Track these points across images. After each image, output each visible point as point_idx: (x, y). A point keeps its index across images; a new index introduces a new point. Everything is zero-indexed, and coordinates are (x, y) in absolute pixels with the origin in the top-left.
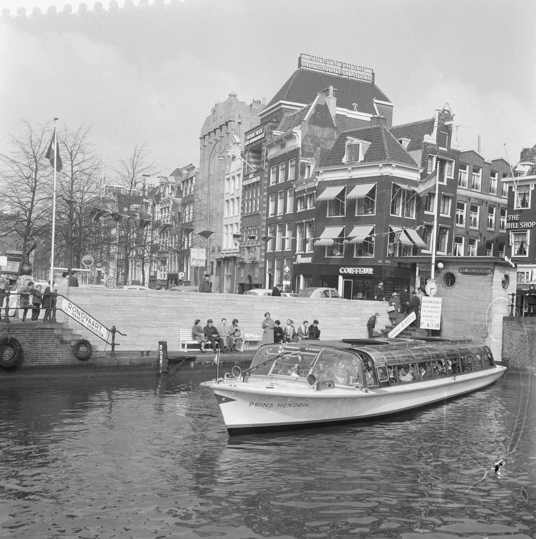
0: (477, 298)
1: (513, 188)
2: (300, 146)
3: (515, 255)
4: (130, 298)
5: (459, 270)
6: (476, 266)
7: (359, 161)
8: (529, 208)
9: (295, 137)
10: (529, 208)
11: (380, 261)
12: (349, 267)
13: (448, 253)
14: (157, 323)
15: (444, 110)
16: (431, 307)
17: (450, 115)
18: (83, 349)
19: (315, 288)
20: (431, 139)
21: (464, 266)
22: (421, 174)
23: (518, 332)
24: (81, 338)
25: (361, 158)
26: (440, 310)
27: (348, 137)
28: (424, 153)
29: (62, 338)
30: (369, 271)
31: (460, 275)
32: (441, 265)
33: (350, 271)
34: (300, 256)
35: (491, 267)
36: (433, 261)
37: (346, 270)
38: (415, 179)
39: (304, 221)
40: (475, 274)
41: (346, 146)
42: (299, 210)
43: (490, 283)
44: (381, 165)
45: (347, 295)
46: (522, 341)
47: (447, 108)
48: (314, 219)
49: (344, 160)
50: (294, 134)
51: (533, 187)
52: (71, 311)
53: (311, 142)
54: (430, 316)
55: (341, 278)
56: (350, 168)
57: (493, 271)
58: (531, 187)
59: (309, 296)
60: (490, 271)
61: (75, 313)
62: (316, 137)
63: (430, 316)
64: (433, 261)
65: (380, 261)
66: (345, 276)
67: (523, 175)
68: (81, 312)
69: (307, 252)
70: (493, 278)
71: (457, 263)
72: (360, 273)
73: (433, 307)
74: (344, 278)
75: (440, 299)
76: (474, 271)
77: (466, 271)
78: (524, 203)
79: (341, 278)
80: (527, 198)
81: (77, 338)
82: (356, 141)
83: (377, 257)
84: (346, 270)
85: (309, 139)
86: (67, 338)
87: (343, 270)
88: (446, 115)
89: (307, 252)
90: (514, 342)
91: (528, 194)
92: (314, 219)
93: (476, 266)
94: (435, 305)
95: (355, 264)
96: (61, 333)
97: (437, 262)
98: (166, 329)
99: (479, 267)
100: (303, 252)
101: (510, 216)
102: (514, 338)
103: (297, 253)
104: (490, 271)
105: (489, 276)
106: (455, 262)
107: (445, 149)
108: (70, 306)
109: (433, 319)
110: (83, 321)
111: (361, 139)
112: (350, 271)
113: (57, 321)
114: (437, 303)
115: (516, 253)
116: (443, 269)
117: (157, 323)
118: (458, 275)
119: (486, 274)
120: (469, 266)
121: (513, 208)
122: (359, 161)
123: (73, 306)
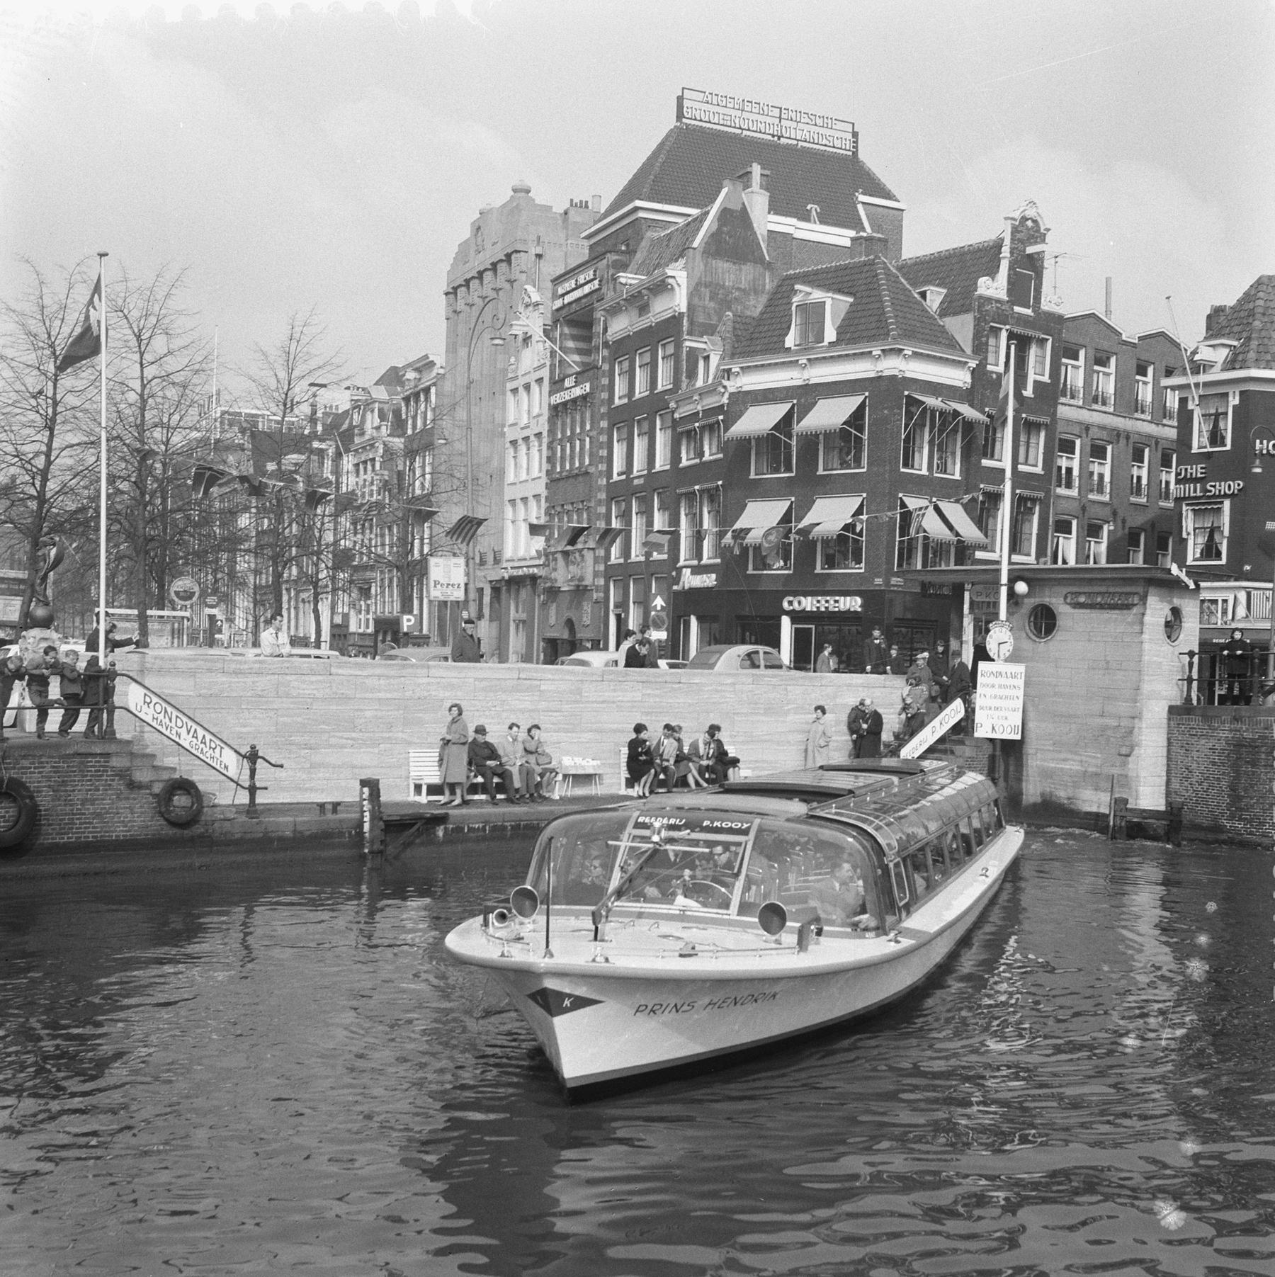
0: (1108, 662)
1: (1190, 402)
2: (684, 309)
3: (1195, 560)
4: (288, 678)
5: (1066, 597)
6: (1103, 589)
7: (826, 343)
8: (1228, 447)
9: (673, 288)
10: (1228, 447)
11: (878, 581)
12: (805, 594)
13: (1037, 558)
14: (354, 735)
15: (1024, 219)
16: (1000, 686)
17: (1038, 231)
18: (180, 800)
19: (723, 646)
20: (994, 287)
21: (1075, 589)
22: (973, 372)
23: (1203, 742)
24: (177, 776)
25: (830, 335)
26: (1021, 693)
27: (797, 287)
28: (978, 321)
29: (130, 775)
30: (853, 604)
31: (1068, 609)
32: (1021, 587)
33: (808, 604)
34: (689, 570)
35: (1140, 590)
36: (1004, 579)
37: (799, 603)
38: (960, 384)
39: (697, 487)
40: (1102, 607)
41: (794, 308)
42: (685, 463)
43: (1137, 628)
44: (876, 352)
45: (803, 660)
46: (1214, 763)
47: (1031, 213)
48: (720, 483)
49: (790, 341)
50: (670, 281)
51: (1237, 398)
52: (151, 711)
53: (711, 299)
55: (786, 621)
56: (803, 361)
57: (1144, 599)
58: (1231, 398)
59: (712, 666)
60: (1136, 600)
61: (161, 717)
62: (723, 286)
64: (1004, 579)
65: (878, 581)
66: (797, 617)
67: (1214, 370)
68: (175, 713)
69: (705, 561)
70: (1143, 614)
71: (1060, 582)
72: (831, 609)
73: (1005, 687)
74: (793, 621)
75: (1020, 668)
77: (1082, 599)
79: (786, 621)
80: (1221, 425)
81: (165, 776)
82: (817, 295)
83: (872, 571)
84: (799, 603)
85: (706, 292)
86: (142, 776)
87: (790, 603)
88: (1028, 229)
89: (705, 561)
90: (1194, 765)
91: (1226, 414)
92: (720, 483)
93: (1103, 589)
94: (1010, 682)
95: (820, 587)
96: (128, 764)
97: (1012, 581)
98: (376, 751)
99: (1111, 590)
100: (695, 562)
102: (1195, 754)
103: (682, 563)
104: (1136, 600)
105: (1135, 610)
106: (1055, 579)
107: (1029, 312)
108: (148, 700)
109: (1003, 713)
110: (178, 735)
111: (829, 290)
112: (808, 604)
113: (118, 736)
114: (1014, 676)
115: (1198, 555)
116: (1028, 595)
117: (354, 735)
118: (1062, 609)
119: (1128, 607)
120: (1086, 590)
121: (1190, 448)
122: (826, 343)
123: (155, 699)
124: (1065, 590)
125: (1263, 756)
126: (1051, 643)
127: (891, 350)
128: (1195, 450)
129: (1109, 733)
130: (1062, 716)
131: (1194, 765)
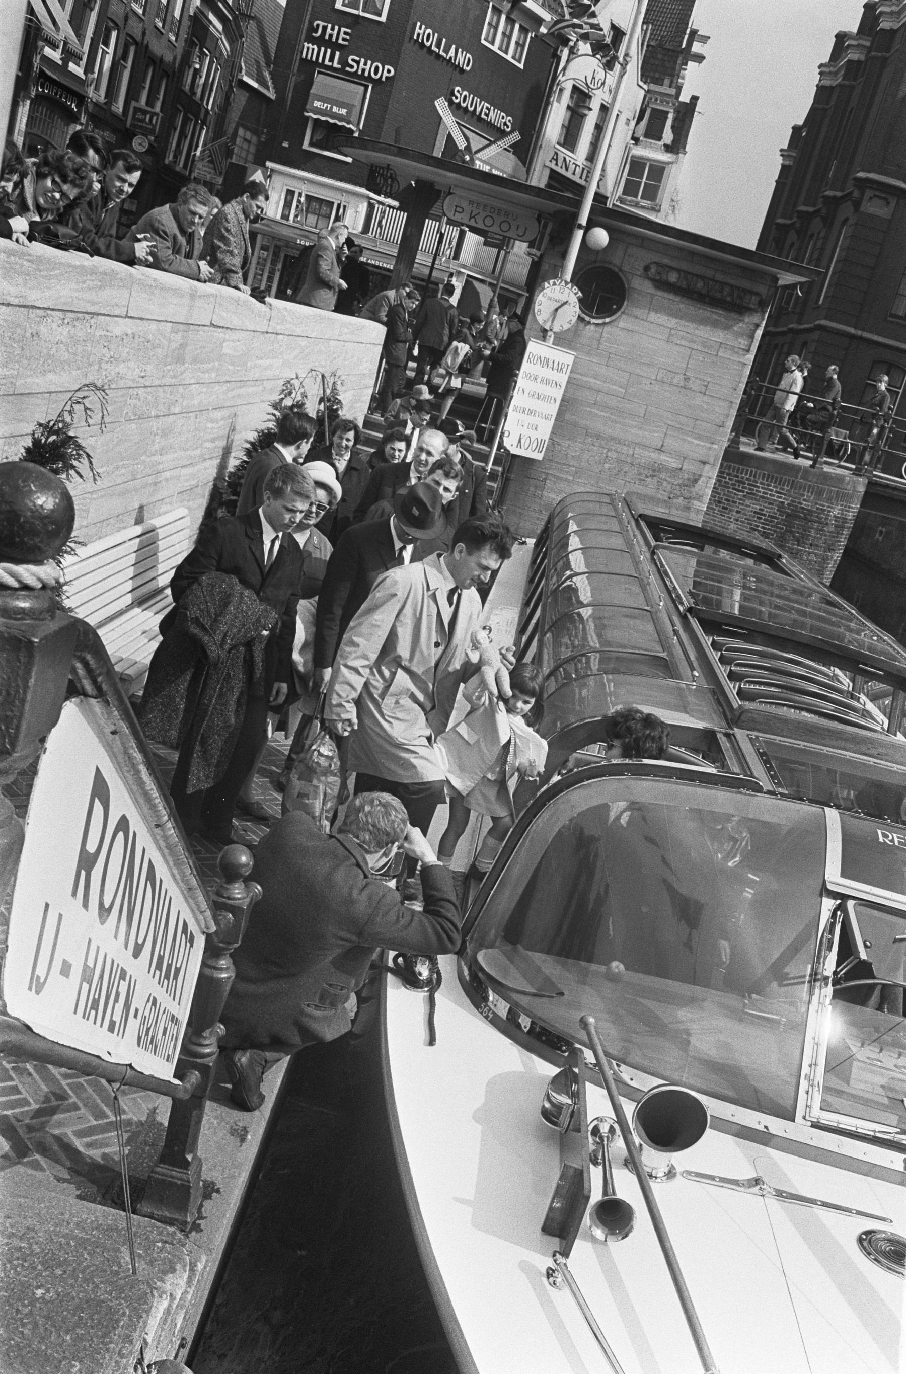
0: (687, 379)
5: (647, 269)
6: (709, 273)
8: (383, 18)
10: (383, 18)
21: (666, 261)
23: (748, 502)
26: (558, 394)
30: (349, 160)
31: (647, 287)
32: (601, 236)
36: (583, 220)
54: (531, 412)
63: (531, 412)
64: (583, 220)
70: (757, 326)
76: (700, 285)
77: (673, 278)
99: (719, 277)
101: (322, 24)
124: (649, 257)
125: (813, 533)
126: (607, 329)
129: (663, 476)
130: (598, 437)
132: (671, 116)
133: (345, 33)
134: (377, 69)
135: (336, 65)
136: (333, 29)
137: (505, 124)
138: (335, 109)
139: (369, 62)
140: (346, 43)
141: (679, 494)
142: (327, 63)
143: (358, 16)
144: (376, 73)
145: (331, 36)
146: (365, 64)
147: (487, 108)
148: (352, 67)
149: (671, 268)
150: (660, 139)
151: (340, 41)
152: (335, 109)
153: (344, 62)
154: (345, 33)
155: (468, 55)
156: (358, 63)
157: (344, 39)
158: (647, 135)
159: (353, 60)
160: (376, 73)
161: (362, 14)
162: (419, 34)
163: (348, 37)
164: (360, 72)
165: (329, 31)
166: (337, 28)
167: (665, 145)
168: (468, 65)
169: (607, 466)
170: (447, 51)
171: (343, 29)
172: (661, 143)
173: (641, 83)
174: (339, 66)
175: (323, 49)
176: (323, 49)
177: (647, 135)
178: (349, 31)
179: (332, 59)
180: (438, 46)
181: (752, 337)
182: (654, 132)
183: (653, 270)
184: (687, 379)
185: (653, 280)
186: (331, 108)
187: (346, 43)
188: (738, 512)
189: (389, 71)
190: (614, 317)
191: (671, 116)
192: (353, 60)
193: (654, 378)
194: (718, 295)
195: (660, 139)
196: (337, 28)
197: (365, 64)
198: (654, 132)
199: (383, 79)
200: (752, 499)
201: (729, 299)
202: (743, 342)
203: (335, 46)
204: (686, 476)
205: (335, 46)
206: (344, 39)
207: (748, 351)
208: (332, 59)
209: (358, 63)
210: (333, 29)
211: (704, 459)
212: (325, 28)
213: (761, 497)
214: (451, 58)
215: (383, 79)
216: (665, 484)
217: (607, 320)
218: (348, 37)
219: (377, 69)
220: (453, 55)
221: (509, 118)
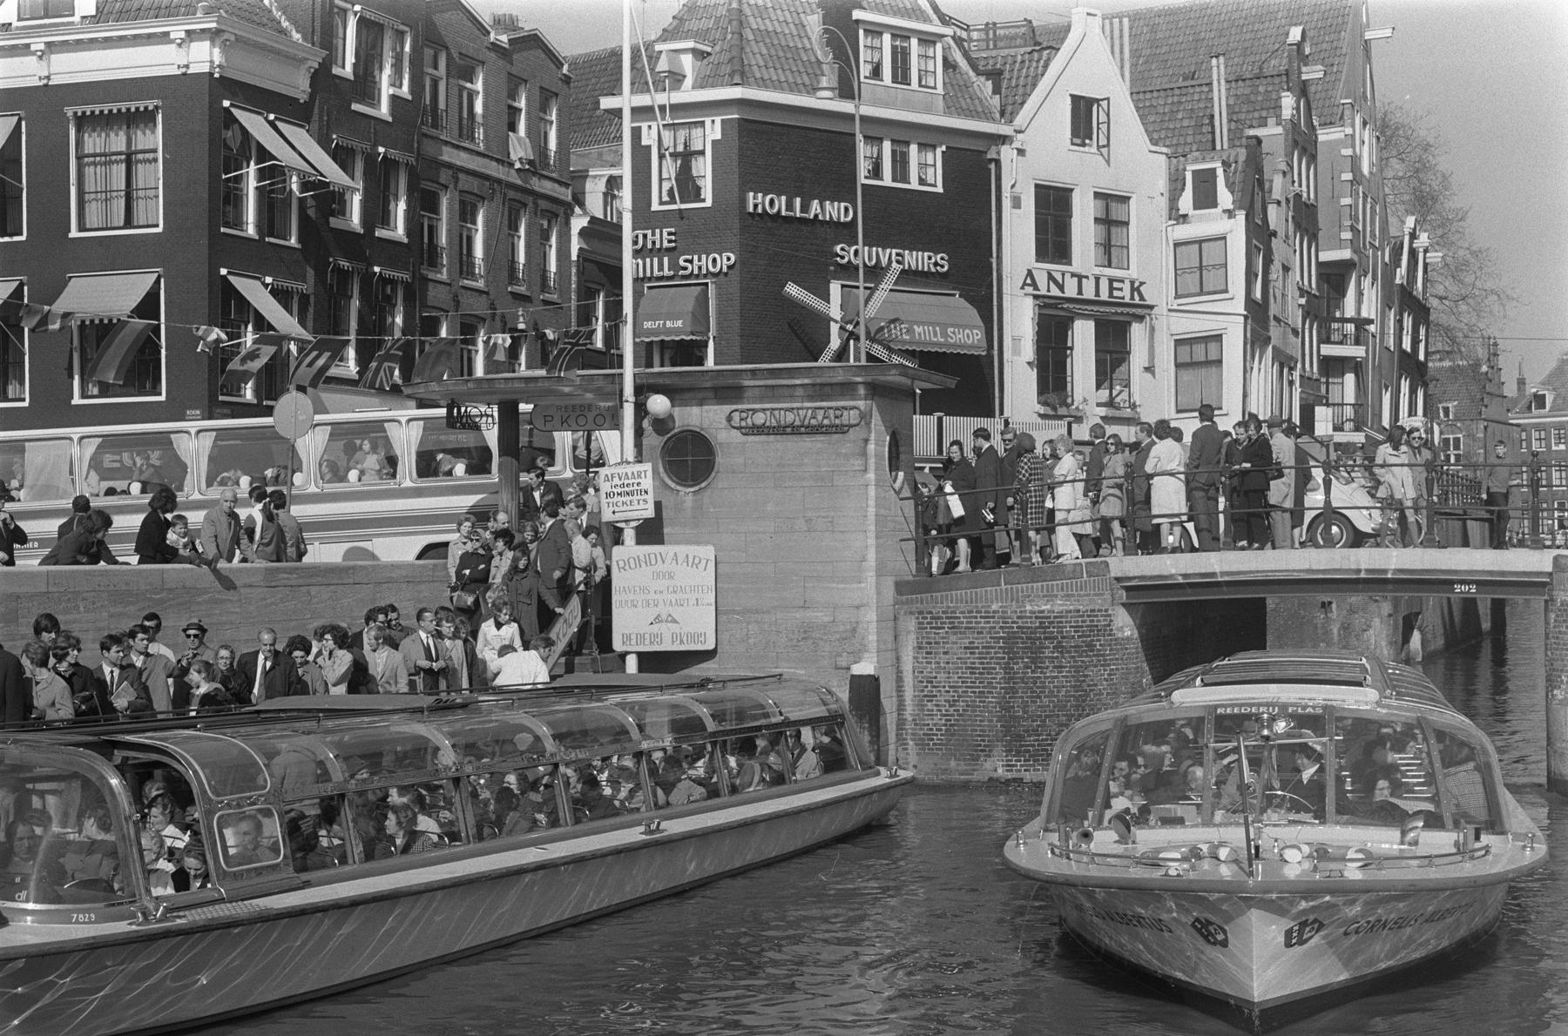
5: (729, 419)
8: (708, 203)
46: (972, 669)
56: (38, 44)
70: (866, 441)
78: (687, 185)
90: (942, 676)
97: (642, 391)
119: (842, 429)
126: (708, 493)
127: (203, 30)
128: (655, 206)
131: (942, 676)
132: (1220, 172)
133: (669, 234)
134: (714, 260)
135: (666, 272)
136: (653, 234)
137: (936, 264)
138: (669, 324)
139: (704, 257)
140: (673, 245)
141: (840, 650)
142: (656, 273)
143: (680, 210)
144: (714, 266)
145: (654, 243)
146: (700, 260)
147: (897, 255)
148: (686, 269)
149: (755, 411)
150: (1214, 205)
151: (666, 244)
152: (669, 324)
153: (674, 265)
154: (669, 234)
155: (843, 205)
156: (691, 262)
157: (670, 241)
158: (1198, 205)
159: (686, 261)
160: (714, 266)
161: (684, 206)
162: (756, 206)
163: (673, 238)
164: (696, 272)
165: (649, 236)
166: (658, 231)
167: (1224, 211)
168: (846, 215)
169: (751, 641)
170: (805, 208)
171: (665, 231)
172: (1219, 209)
173: (1154, 148)
174: (672, 273)
175: (648, 260)
176: (648, 260)
177: (1198, 205)
178: (673, 230)
179: (661, 268)
180: (790, 207)
181: (864, 454)
182: (1205, 198)
183: (736, 416)
184: (808, 521)
185: (739, 428)
186: (665, 324)
187: (673, 245)
188: (945, 653)
189: (729, 259)
190: (710, 480)
191: (1220, 172)
192: (686, 261)
193: (772, 529)
194: (813, 422)
195: (1214, 205)
196: (658, 231)
197: (700, 260)
198: (1205, 198)
199: (725, 269)
200: (955, 634)
201: (826, 422)
202: (857, 463)
203: (661, 252)
204: (841, 628)
205: (661, 252)
206: (670, 241)
207: (865, 470)
208: (661, 268)
209: (691, 262)
210: (653, 234)
211: (856, 603)
212: (645, 236)
213: (966, 628)
214: (816, 216)
215: (725, 269)
216: (822, 643)
217: (703, 485)
218: (673, 238)
219: (714, 260)
220: (819, 211)
221: (939, 256)
